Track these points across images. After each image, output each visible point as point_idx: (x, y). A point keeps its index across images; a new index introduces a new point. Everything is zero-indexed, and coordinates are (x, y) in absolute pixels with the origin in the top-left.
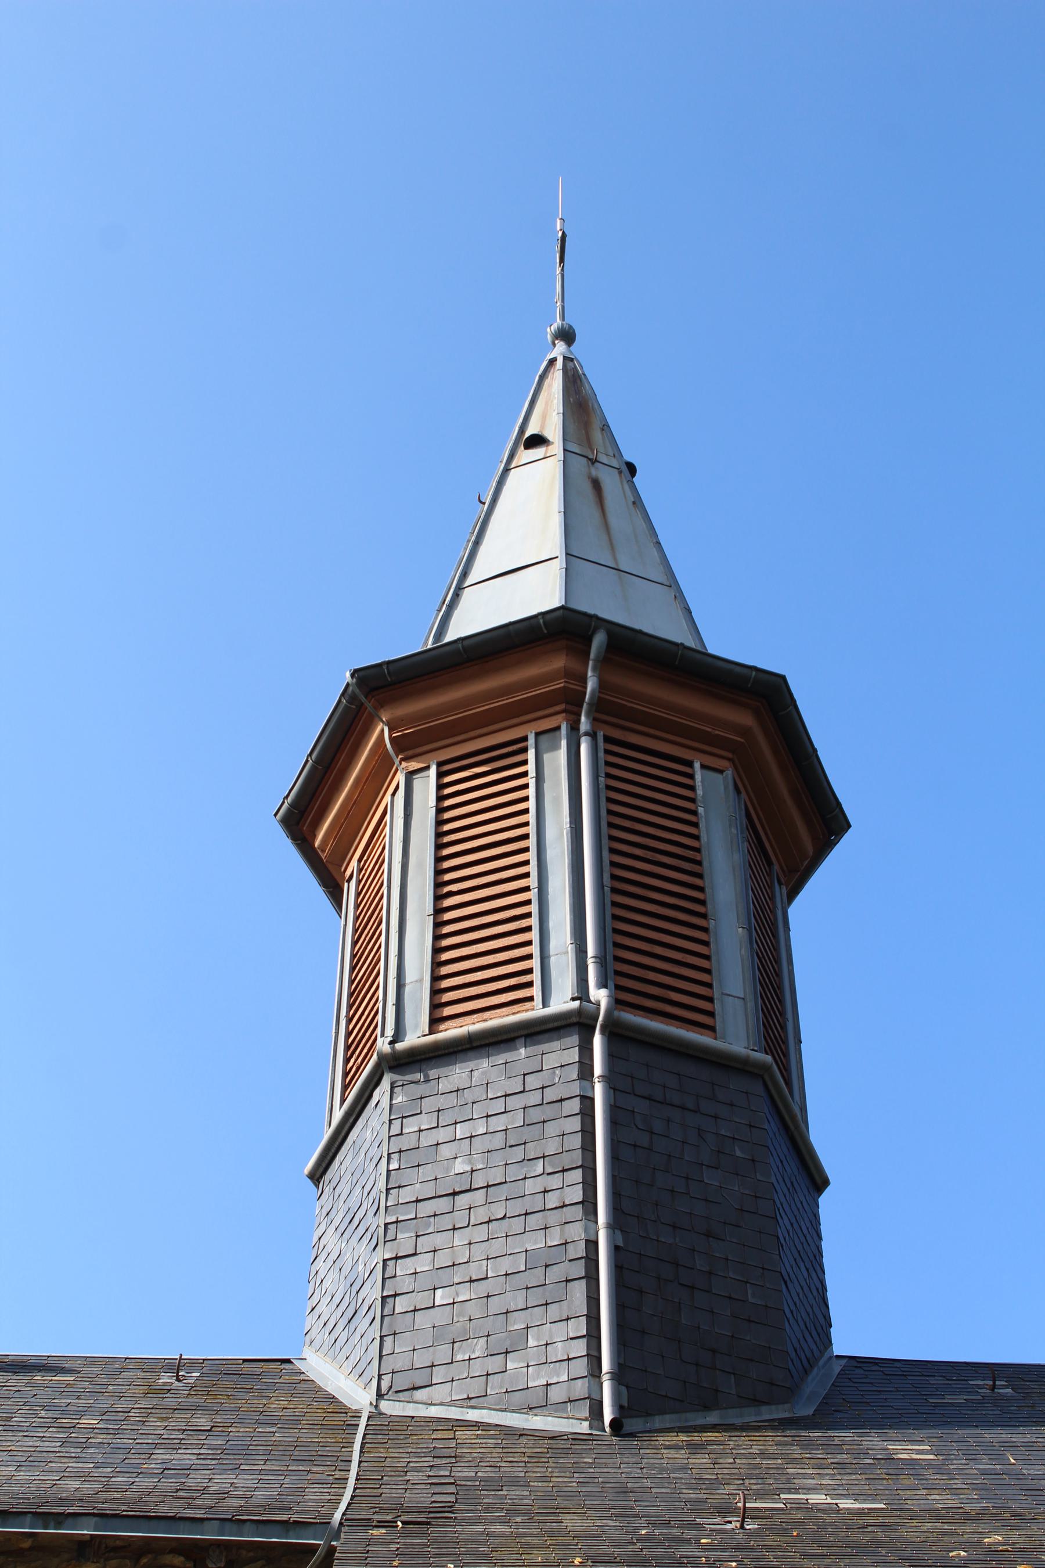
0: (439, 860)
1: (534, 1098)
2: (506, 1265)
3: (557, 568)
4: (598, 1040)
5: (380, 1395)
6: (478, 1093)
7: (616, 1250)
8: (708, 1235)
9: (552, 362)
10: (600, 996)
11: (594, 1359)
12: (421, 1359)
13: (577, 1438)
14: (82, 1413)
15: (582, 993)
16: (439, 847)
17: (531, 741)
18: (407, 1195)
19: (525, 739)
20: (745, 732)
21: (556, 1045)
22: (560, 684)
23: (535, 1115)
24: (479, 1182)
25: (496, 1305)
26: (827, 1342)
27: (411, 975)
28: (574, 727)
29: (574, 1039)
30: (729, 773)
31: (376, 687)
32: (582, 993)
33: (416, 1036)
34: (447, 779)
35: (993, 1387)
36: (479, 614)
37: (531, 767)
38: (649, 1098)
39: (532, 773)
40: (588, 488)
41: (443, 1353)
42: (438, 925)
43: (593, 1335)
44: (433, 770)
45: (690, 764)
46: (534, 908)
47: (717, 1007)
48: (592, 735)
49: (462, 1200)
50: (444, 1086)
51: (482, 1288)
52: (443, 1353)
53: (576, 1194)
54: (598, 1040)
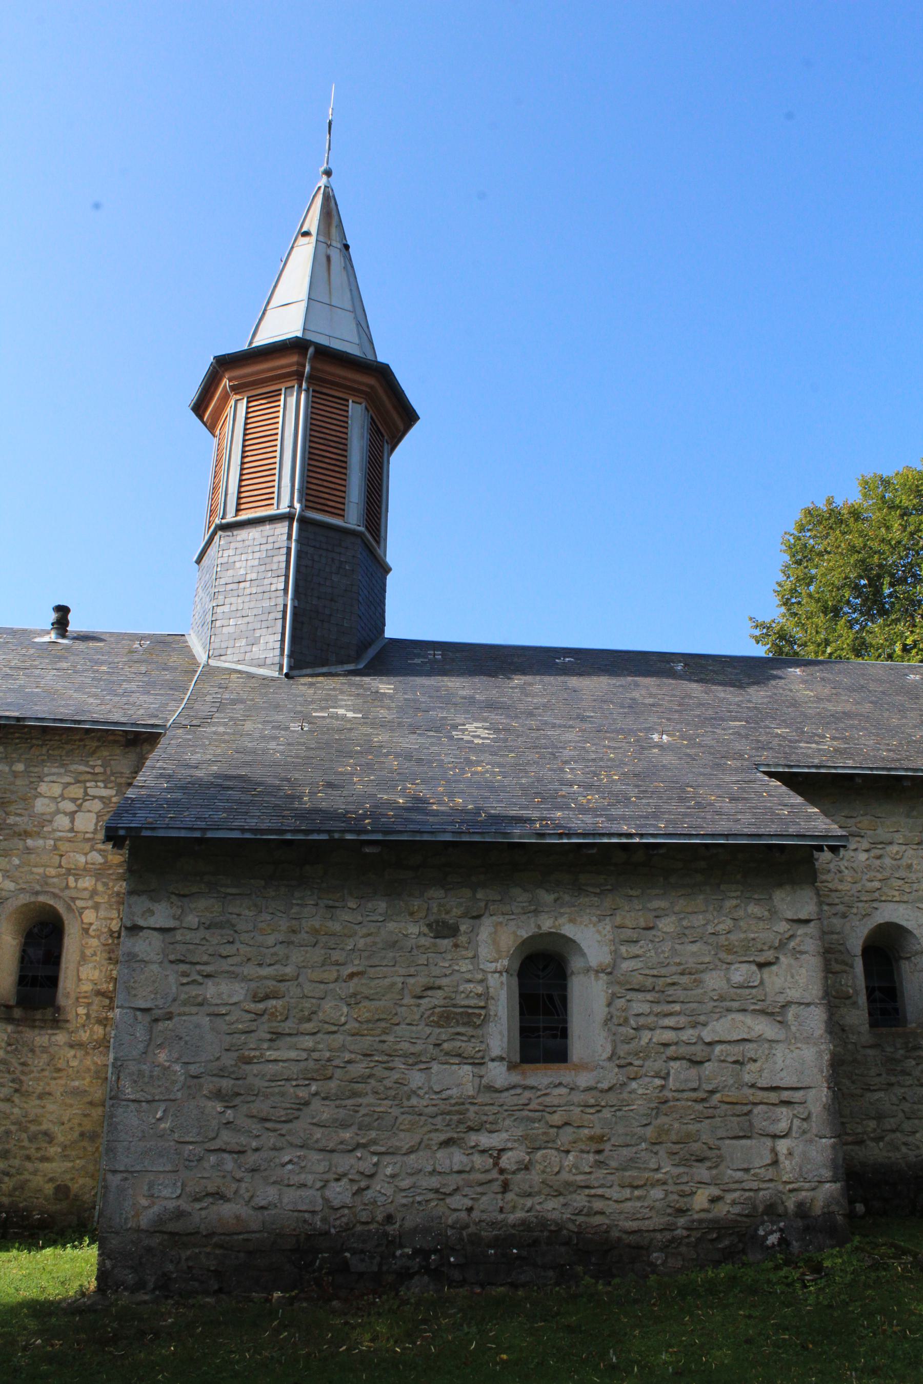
0: (244, 440)
1: (270, 546)
2: (255, 612)
3: (304, 305)
4: (295, 524)
5: (209, 657)
6: (250, 543)
7: (294, 608)
8: (332, 600)
9: (320, 188)
10: (297, 506)
11: (282, 649)
12: (224, 645)
13: (273, 679)
14: (102, 664)
15: (291, 506)
16: (245, 435)
17: (283, 392)
18: (223, 581)
19: (281, 390)
20: (371, 387)
21: (280, 525)
22: (294, 368)
23: (270, 553)
24: (248, 578)
25: (251, 627)
26: (383, 631)
27: (230, 491)
28: (300, 386)
29: (286, 524)
30: (364, 405)
31: (224, 363)
32: (291, 506)
33: (230, 518)
34: (251, 405)
35: (434, 655)
36: (267, 336)
37: (282, 403)
38: (314, 547)
39: (282, 406)
40: (324, 260)
41: (231, 643)
42: (242, 469)
43: (282, 641)
44: (245, 400)
45: (348, 401)
46: (277, 466)
47: (346, 507)
48: (307, 390)
49: (242, 585)
50: (239, 538)
51: (246, 620)
52: (231, 643)
53: (282, 586)
54: (295, 524)
